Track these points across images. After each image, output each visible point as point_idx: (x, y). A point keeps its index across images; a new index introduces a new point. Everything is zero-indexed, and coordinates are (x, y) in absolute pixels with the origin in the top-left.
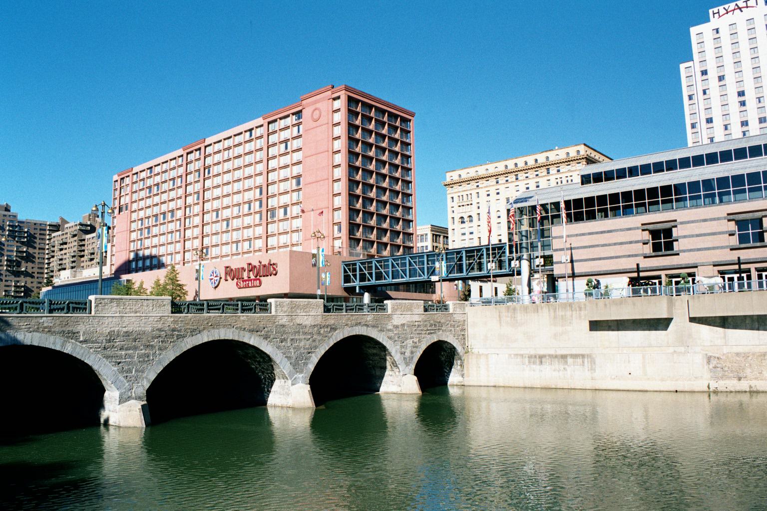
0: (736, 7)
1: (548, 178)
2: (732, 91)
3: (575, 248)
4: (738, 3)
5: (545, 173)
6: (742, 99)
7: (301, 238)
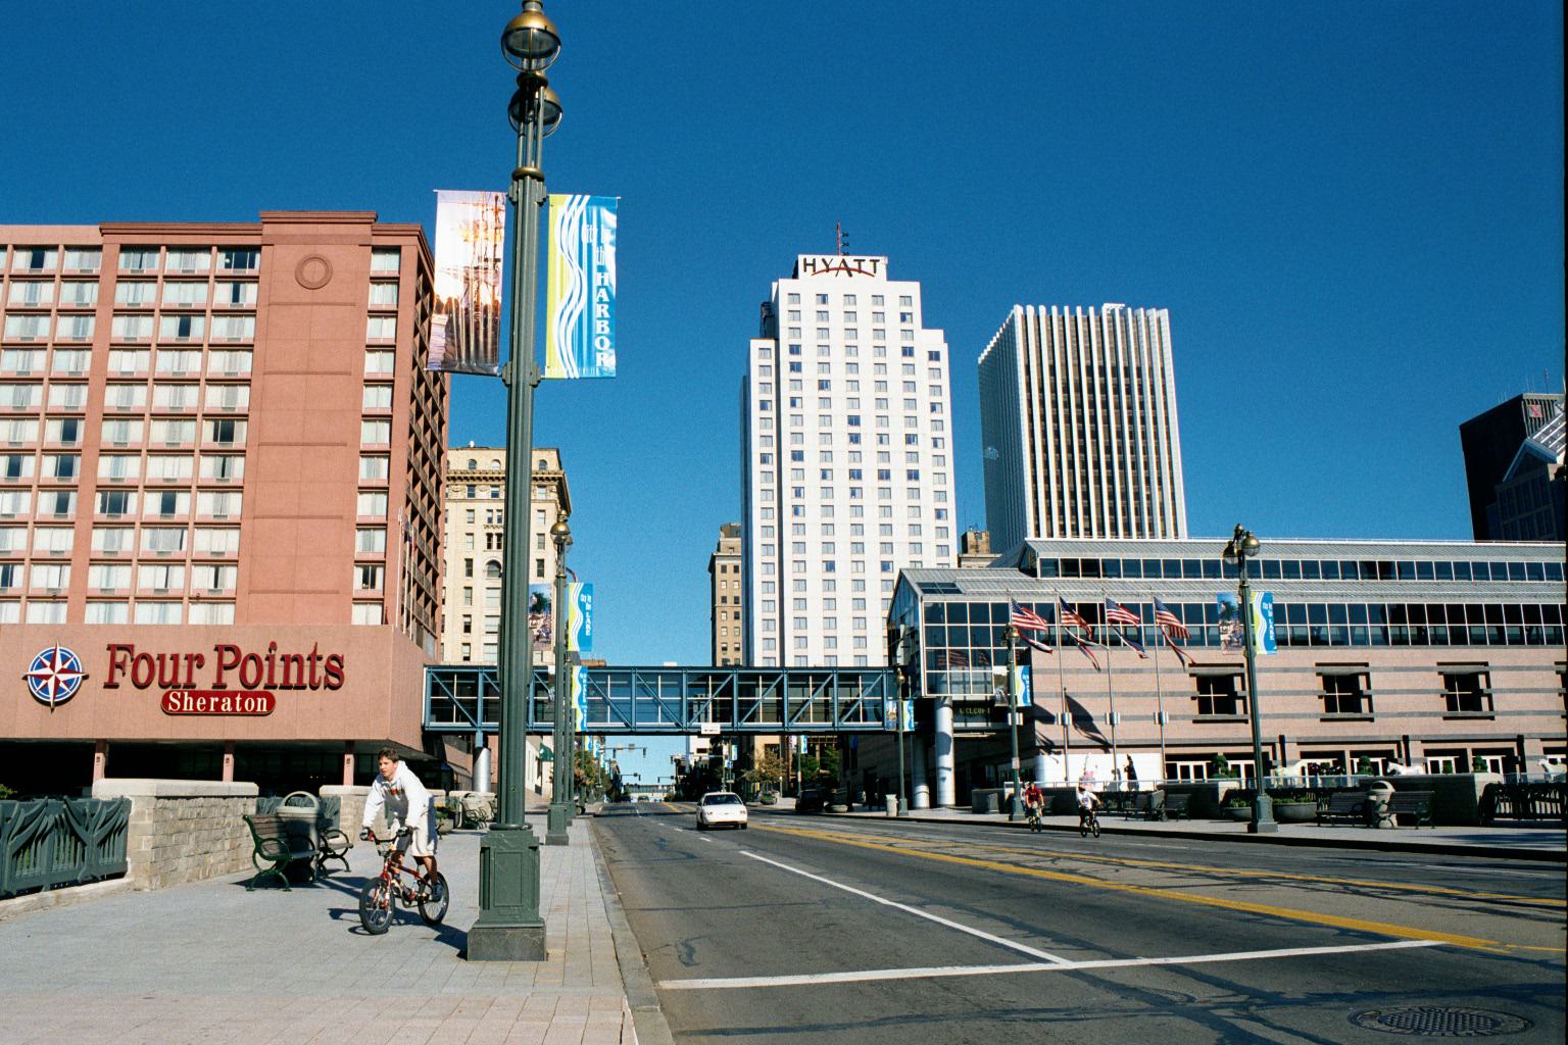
0: (843, 266)
1: (471, 506)
2: (840, 411)
3: (1101, 695)
4: (847, 258)
5: (463, 494)
6: (854, 430)
7: (66, 583)
